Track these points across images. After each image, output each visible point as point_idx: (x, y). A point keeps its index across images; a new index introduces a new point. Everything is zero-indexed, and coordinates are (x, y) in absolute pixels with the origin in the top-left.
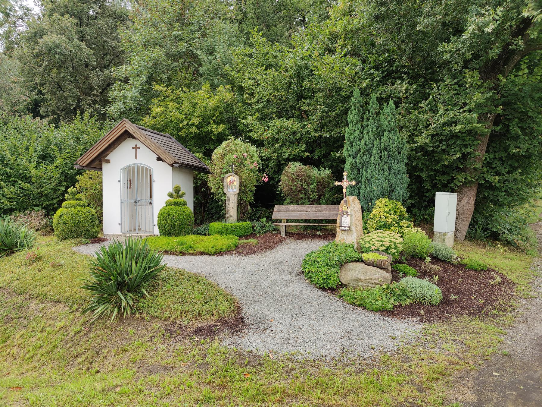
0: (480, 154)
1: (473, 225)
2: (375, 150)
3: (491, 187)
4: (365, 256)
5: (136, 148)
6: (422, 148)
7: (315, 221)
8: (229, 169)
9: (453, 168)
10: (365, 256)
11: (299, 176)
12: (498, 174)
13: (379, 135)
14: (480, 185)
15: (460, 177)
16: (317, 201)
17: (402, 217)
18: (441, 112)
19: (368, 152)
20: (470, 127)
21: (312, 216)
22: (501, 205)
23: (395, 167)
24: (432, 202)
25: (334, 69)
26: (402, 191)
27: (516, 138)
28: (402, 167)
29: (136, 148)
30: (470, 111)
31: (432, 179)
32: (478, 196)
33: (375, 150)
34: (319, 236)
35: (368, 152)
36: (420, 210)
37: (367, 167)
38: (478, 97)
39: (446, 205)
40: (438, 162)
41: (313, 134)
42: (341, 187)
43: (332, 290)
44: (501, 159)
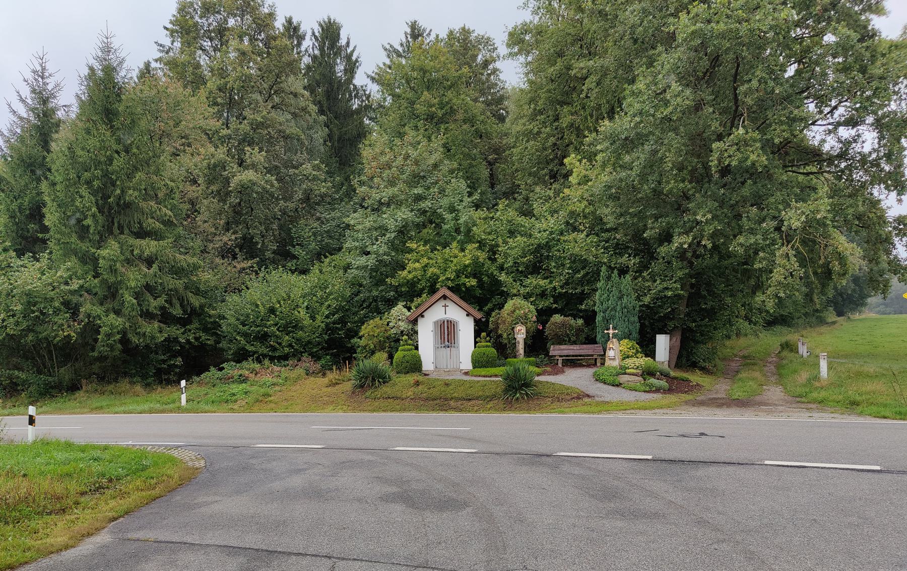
0: (683, 308)
1: (680, 357)
2: (618, 308)
3: (690, 330)
4: (628, 371)
5: (445, 306)
6: (648, 307)
7: (576, 356)
8: (518, 320)
9: (667, 317)
10: (628, 371)
11: (563, 325)
12: (695, 321)
13: (620, 298)
14: (683, 329)
15: (671, 324)
16: (575, 343)
17: (637, 352)
18: (658, 282)
19: (614, 309)
20: (676, 292)
21: (577, 353)
22: (698, 342)
23: (632, 319)
24: (654, 343)
25: (579, 243)
26: (635, 335)
27: (704, 297)
28: (636, 319)
29: (445, 306)
30: (675, 282)
31: (652, 324)
32: (682, 336)
33: (618, 308)
34: (584, 366)
35: (614, 309)
36: (648, 348)
37: (614, 320)
38: (680, 274)
39: (662, 342)
40: (656, 314)
41: (559, 290)
42: (608, 334)
43: (617, 386)
44: (696, 311)
